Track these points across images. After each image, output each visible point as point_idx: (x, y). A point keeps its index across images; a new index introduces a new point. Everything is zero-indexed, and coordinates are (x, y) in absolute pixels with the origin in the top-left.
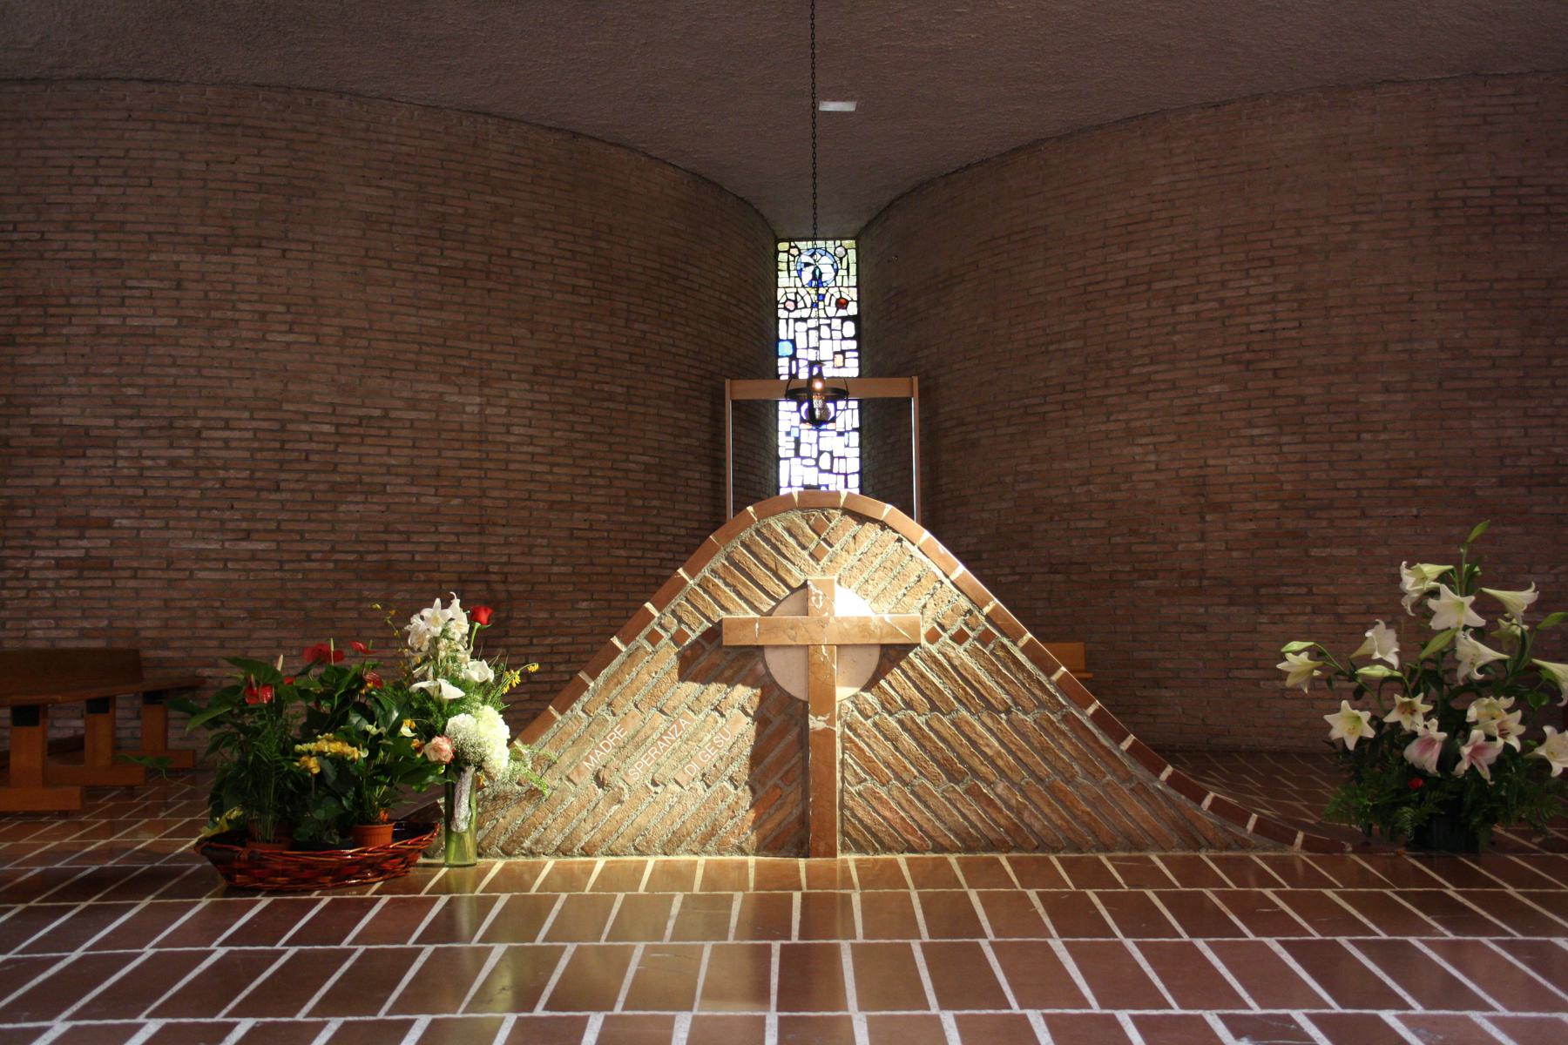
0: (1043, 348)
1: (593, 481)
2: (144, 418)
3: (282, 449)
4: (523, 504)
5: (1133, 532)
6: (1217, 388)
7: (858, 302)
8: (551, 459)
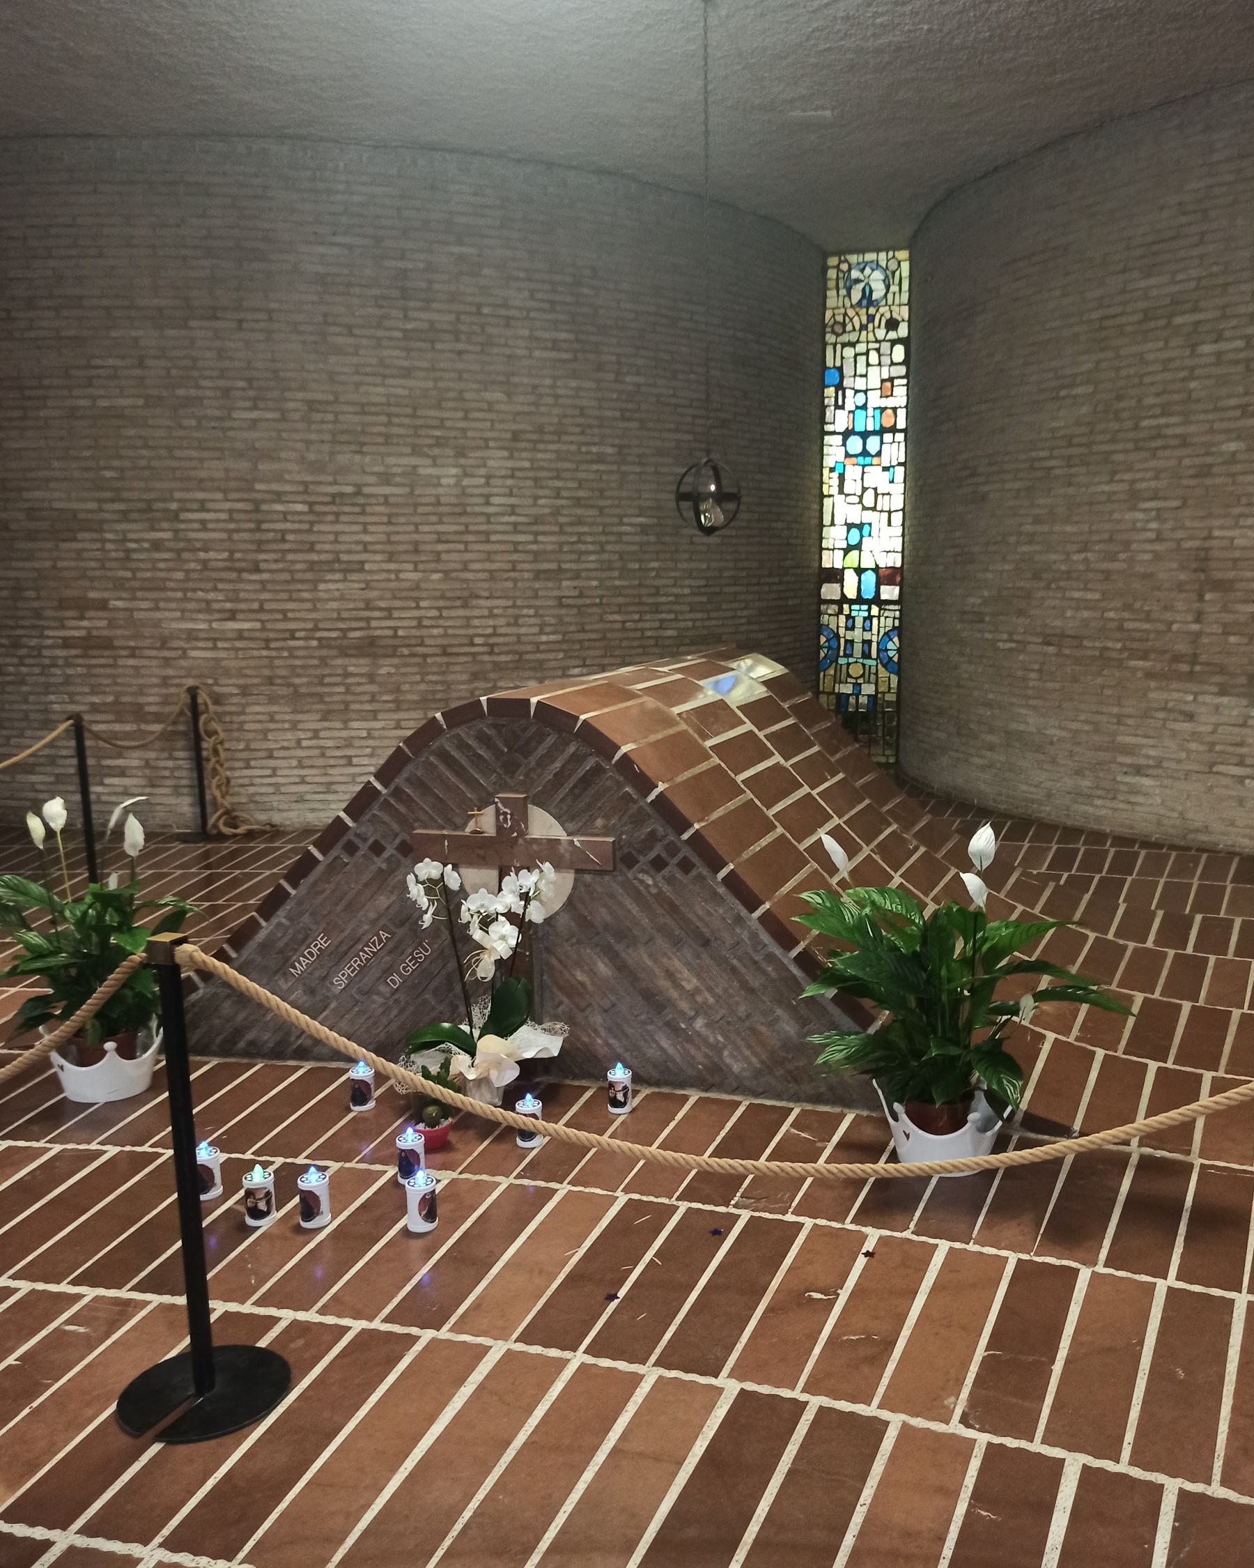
0: (1054, 394)
1: (583, 547)
2: (123, 501)
3: (258, 529)
4: (507, 575)
5: (1128, 607)
6: (1233, 446)
7: (909, 321)
8: (535, 528)
